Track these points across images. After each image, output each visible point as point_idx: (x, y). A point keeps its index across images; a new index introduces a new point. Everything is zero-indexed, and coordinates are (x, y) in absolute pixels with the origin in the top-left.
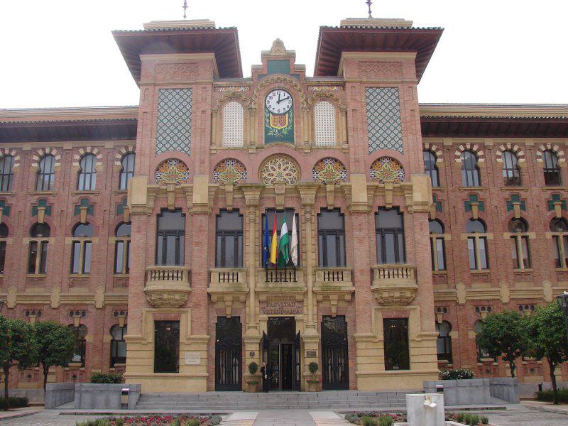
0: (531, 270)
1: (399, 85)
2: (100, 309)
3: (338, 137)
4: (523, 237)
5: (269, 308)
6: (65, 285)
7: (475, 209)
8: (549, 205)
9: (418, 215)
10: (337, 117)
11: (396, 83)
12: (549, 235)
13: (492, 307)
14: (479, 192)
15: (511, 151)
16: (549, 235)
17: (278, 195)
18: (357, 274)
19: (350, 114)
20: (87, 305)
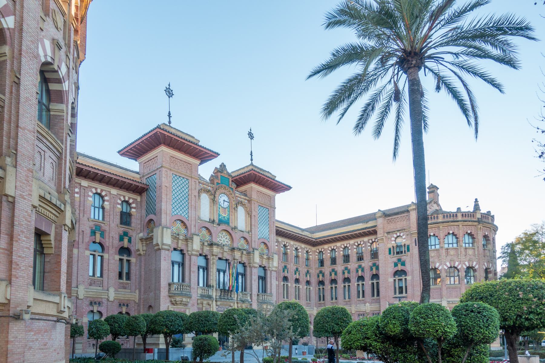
0: (129, 282)
1: (269, 208)
2: (112, 301)
3: (246, 228)
4: (127, 260)
5: (219, 309)
6: (86, 284)
7: (98, 235)
8: (120, 238)
9: (273, 272)
10: (246, 216)
11: (269, 206)
12: (117, 257)
13: (129, 304)
14: (102, 225)
15: (100, 194)
16: (117, 257)
17: (225, 252)
18: (253, 296)
19: (253, 217)
20: (102, 298)
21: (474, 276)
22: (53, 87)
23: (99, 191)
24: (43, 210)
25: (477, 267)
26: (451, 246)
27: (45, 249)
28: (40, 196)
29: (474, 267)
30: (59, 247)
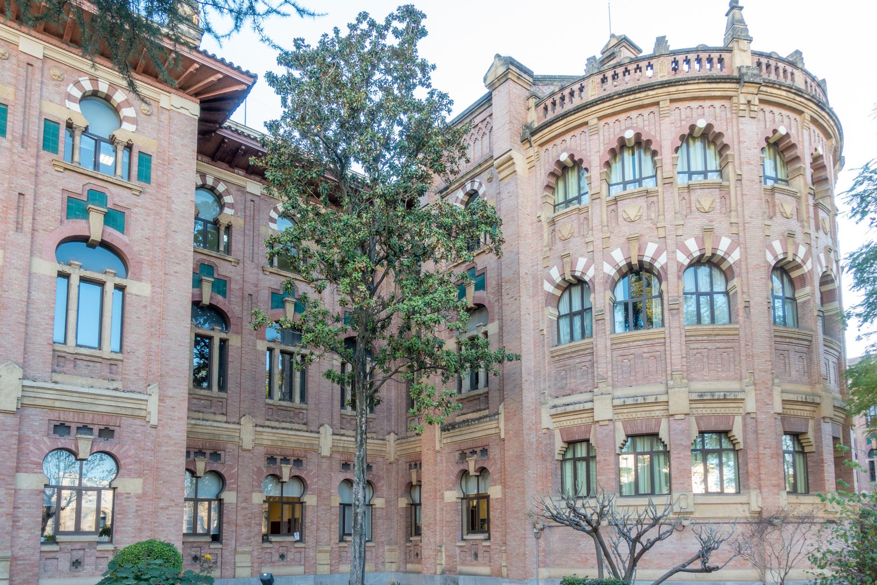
21: (726, 293)
22: (794, 274)
23: (210, 181)
24: (802, 412)
25: (734, 258)
26: (698, 179)
27: (805, 448)
28: (834, 406)
29: (723, 259)
30: (819, 446)
